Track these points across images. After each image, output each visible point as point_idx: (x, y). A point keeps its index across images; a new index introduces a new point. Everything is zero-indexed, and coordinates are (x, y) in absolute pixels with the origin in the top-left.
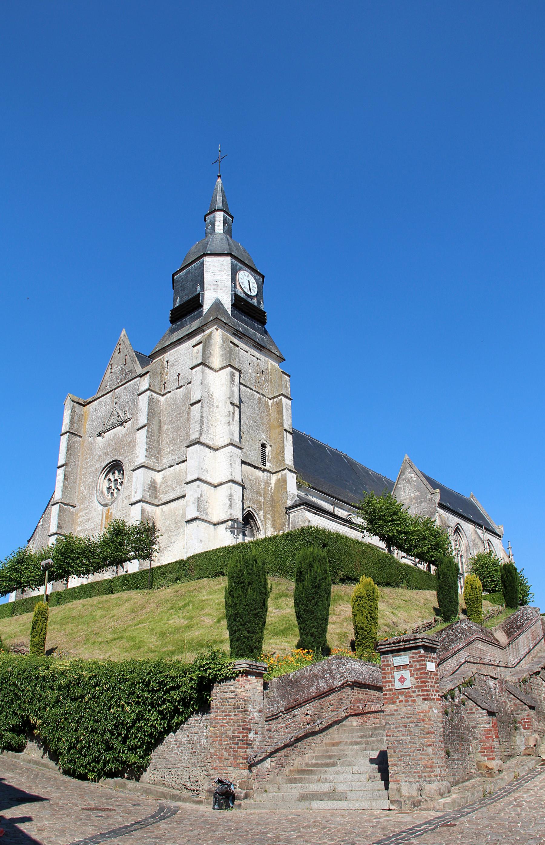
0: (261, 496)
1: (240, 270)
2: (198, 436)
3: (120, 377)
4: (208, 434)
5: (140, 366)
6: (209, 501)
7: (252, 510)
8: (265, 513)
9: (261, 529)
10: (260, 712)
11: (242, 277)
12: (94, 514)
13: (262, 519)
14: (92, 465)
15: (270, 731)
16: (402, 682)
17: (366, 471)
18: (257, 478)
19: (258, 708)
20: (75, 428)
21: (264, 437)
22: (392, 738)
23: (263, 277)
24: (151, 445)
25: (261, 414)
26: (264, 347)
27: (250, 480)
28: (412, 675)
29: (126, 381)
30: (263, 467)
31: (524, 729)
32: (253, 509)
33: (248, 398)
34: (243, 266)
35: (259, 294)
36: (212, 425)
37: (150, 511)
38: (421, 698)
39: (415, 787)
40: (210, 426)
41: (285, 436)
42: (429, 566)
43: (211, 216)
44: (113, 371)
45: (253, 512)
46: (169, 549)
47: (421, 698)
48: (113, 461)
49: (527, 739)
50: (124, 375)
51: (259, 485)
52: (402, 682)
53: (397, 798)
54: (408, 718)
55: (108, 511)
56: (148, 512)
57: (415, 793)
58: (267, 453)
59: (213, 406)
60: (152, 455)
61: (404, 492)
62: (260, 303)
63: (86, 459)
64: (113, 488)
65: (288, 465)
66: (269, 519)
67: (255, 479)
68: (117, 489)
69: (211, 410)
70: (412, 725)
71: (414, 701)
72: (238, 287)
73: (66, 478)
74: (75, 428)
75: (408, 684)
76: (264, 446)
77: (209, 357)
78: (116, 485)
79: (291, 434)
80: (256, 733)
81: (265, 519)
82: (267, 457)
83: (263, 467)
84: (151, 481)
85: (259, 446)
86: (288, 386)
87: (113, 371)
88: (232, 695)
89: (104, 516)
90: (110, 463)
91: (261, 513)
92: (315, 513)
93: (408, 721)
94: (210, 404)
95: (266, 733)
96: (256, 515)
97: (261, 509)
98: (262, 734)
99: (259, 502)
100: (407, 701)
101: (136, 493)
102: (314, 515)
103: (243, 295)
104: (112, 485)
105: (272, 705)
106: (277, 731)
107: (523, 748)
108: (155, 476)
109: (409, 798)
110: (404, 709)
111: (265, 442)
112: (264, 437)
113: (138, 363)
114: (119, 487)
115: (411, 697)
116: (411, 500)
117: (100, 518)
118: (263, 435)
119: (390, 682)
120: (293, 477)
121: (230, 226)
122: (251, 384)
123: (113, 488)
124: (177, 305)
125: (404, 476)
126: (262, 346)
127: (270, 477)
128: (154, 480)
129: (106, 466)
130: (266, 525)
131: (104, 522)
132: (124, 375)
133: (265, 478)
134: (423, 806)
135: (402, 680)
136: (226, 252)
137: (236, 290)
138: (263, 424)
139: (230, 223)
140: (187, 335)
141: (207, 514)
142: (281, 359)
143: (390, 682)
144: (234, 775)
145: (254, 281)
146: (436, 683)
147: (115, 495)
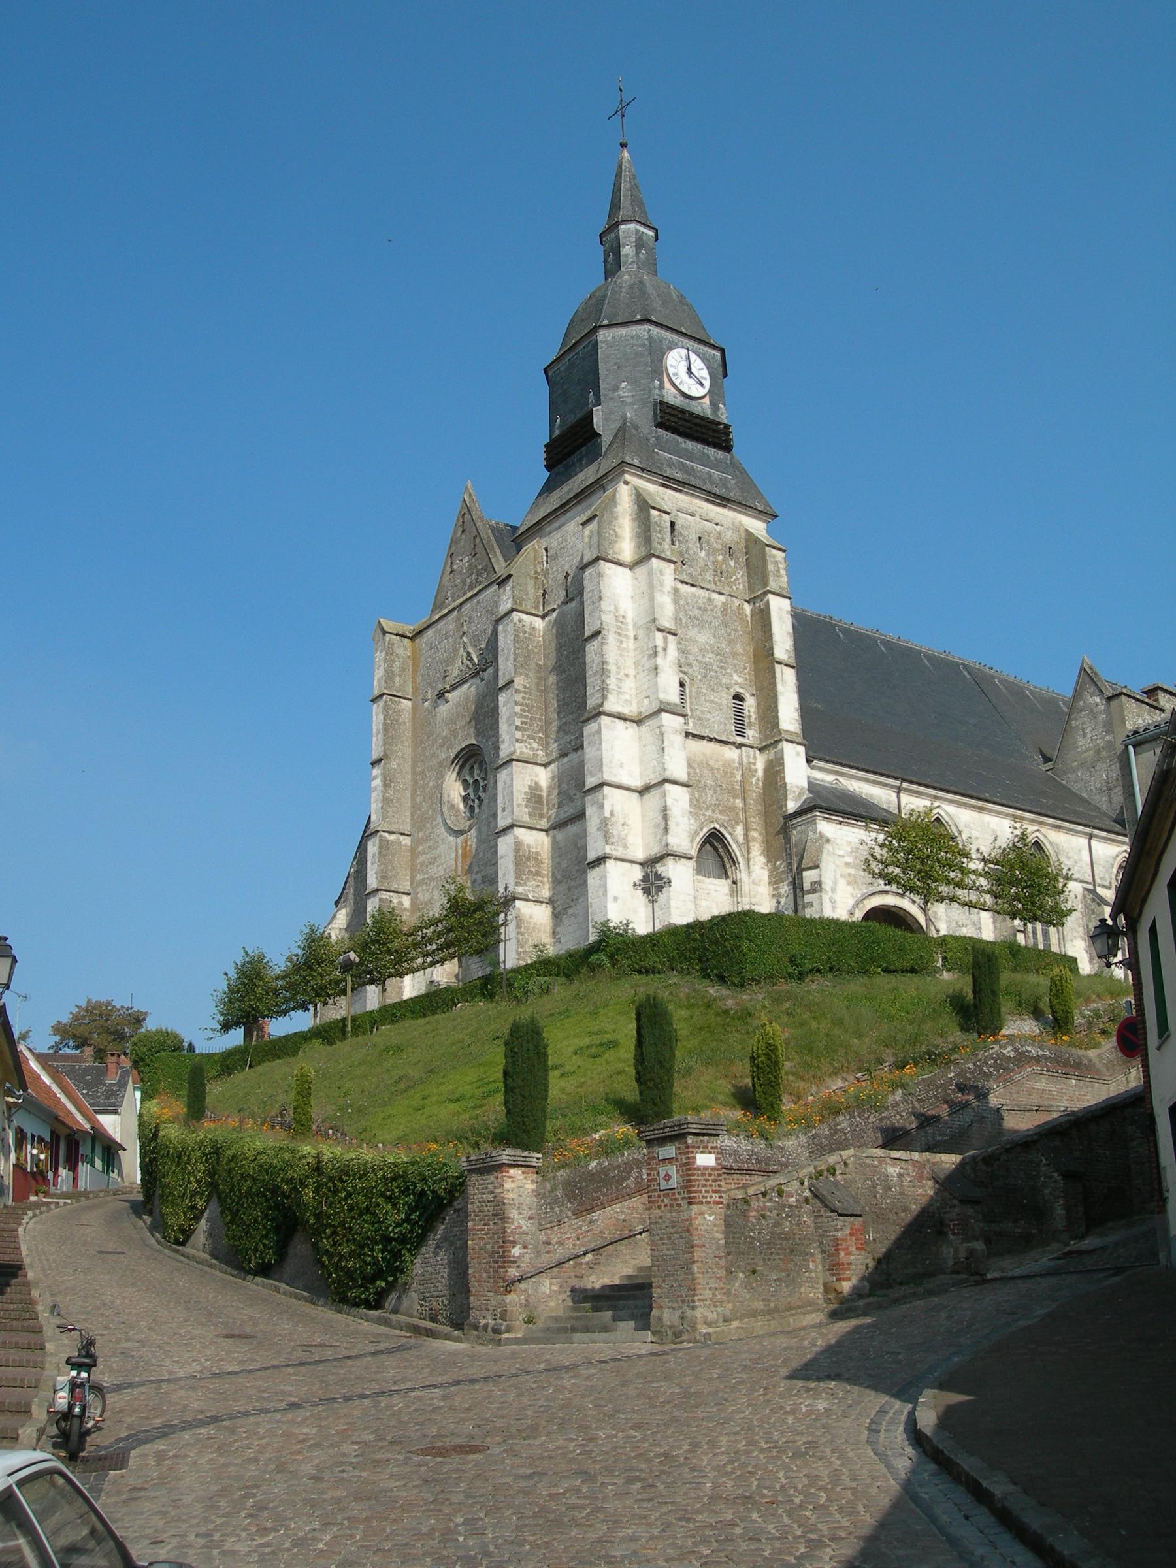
0: (736, 797)
1: (670, 349)
2: (599, 702)
3: (469, 580)
4: (619, 693)
5: (501, 558)
6: (628, 822)
7: (718, 827)
8: (747, 829)
9: (740, 860)
10: (530, 1218)
11: (675, 363)
12: (443, 849)
13: (741, 839)
14: (433, 755)
15: (549, 1244)
16: (667, 1181)
17: (1017, 691)
18: (727, 764)
19: (527, 1213)
20: (397, 684)
21: (739, 680)
22: (656, 1253)
23: (722, 351)
24: (526, 717)
25: (729, 635)
26: (728, 500)
27: (712, 769)
28: (678, 1172)
29: (479, 588)
30: (739, 740)
31: (953, 1234)
32: (722, 826)
33: (700, 608)
34: (675, 337)
35: (716, 393)
36: (627, 675)
37: (532, 843)
38: (686, 1201)
39: (678, 1314)
40: (623, 678)
41: (778, 674)
42: (1025, 924)
43: (613, 235)
44: (455, 567)
45: (722, 830)
46: (570, 911)
47: (686, 1201)
48: (467, 746)
49: (956, 1250)
50: (474, 576)
51: (733, 775)
52: (667, 1181)
53: (658, 1328)
54: (673, 1227)
55: (466, 842)
56: (528, 846)
57: (676, 1322)
58: (746, 712)
59: (627, 636)
60: (528, 737)
61: (1084, 735)
62: (719, 408)
63: (422, 742)
64: (472, 796)
65: (786, 731)
66: (755, 839)
67: (724, 765)
68: (479, 798)
69: (624, 645)
70: (677, 1236)
71: (679, 1205)
72: (667, 385)
73: (386, 785)
74: (397, 684)
75: (674, 1183)
76: (738, 697)
77: (613, 542)
78: (476, 791)
79: (793, 667)
80: (525, 1247)
81: (747, 839)
82: (746, 719)
83: (739, 740)
84: (530, 787)
85: (727, 700)
86: (783, 572)
87: (455, 567)
88: (490, 1197)
89: (460, 851)
90: (462, 750)
91: (739, 830)
92: (841, 822)
93: (672, 1230)
94: (620, 634)
95: (541, 1246)
96: (727, 835)
97: (737, 824)
98: (536, 1247)
99: (733, 808)
100: (672, 1205)
101: (504, 810)
102: (839, 826)
103: (678, 401)
104: (470, 791)
105: (552, 1208)
106: (561, 1243)
107: (950, 1263)
108: (537, 776)
109: (671, 1327)
110: (669, 1215)
111: (741, 690)
112: (739, 680)
113: (498, 552)
114: (482, 795)
115: (676, 1199)
116: (1098, 752)
117: (453, 855)
118: (735, 677)
119: (655, 1180)
120: (798, 754)
121: (651, 252)
122: (704, 580)
123: (472, 796)
124: (557, 432)
125: (1081, 703)
126: (724, 499)
127: (755, 758)
128: (536, 783)
129: (457, 756)
130: (748, 852)
131: (459, 864)
132: (474, 576)
133: (745, 760)
134: (684, 1337)
135: (667, 1177)
136: (638, 317)
137: (664, 392)
138: (734, 654)
139: (651, 243)
140: (576, 496)
141: (625, 847)
142: (768, 515)
143: (655, 1180)
144: (494, 1303)
145: (702, 365)
146: (715, 1181)
147: (477, 810)
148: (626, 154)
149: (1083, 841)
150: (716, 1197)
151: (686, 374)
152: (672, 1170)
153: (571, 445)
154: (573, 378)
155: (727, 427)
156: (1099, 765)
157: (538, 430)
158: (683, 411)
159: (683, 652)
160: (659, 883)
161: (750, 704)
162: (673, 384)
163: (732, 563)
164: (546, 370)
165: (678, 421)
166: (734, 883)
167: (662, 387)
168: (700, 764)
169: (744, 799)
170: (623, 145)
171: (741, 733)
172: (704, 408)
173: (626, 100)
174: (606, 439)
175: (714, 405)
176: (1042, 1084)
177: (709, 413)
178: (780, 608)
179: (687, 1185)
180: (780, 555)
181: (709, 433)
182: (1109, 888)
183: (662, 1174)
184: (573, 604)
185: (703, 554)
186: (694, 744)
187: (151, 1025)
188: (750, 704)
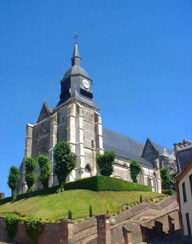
1: (83, 80)
13: (92, 166)
79: (102, 136)
103: (84, 89)
148: (76, 45)
149: (148, 169)
150: (109, 228)
151: (86, 84)
152: (102, 224)
153: (65, 96)
154: (66, 84)
155: (92, 94)
156: (150, 156)
157: (59, 92)
158: (85, 91)
159: (84, 133)
160: (82, 172)
161: (95, 143)
162: (83, 86)
163: (92, 118)
164: (61, 82)
165: (84, 93)
166: (91, 173)
167: (81, 86)
168: (86, 152)
169: (93, 159)
170: (76, 43)
171: (93, 147)
172: (88, 90)
173: (75, 39)
174: (71, 95)
175: (90, 90)
176: (151, 210)
177: (89, 91)
178: (100, 127)
179: (105, 226)
180: (100, 117)
181: (89, 95)
182: (152, 177)
183: (100, 224)
184: (64, 123)
185: (87, 116)
186: (85, 149)
187: (18, 166)
188: (95, 143)
